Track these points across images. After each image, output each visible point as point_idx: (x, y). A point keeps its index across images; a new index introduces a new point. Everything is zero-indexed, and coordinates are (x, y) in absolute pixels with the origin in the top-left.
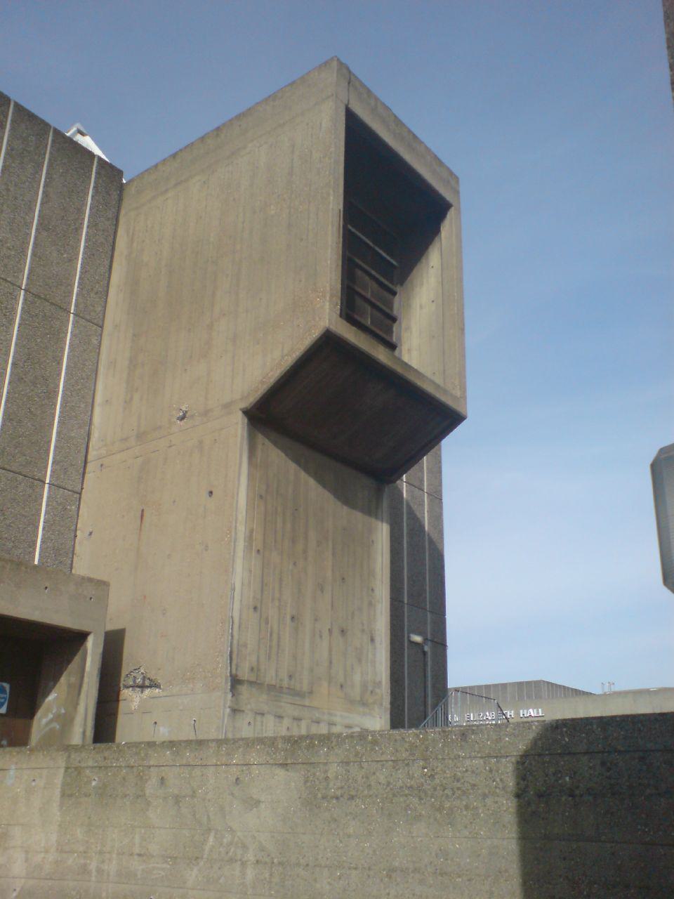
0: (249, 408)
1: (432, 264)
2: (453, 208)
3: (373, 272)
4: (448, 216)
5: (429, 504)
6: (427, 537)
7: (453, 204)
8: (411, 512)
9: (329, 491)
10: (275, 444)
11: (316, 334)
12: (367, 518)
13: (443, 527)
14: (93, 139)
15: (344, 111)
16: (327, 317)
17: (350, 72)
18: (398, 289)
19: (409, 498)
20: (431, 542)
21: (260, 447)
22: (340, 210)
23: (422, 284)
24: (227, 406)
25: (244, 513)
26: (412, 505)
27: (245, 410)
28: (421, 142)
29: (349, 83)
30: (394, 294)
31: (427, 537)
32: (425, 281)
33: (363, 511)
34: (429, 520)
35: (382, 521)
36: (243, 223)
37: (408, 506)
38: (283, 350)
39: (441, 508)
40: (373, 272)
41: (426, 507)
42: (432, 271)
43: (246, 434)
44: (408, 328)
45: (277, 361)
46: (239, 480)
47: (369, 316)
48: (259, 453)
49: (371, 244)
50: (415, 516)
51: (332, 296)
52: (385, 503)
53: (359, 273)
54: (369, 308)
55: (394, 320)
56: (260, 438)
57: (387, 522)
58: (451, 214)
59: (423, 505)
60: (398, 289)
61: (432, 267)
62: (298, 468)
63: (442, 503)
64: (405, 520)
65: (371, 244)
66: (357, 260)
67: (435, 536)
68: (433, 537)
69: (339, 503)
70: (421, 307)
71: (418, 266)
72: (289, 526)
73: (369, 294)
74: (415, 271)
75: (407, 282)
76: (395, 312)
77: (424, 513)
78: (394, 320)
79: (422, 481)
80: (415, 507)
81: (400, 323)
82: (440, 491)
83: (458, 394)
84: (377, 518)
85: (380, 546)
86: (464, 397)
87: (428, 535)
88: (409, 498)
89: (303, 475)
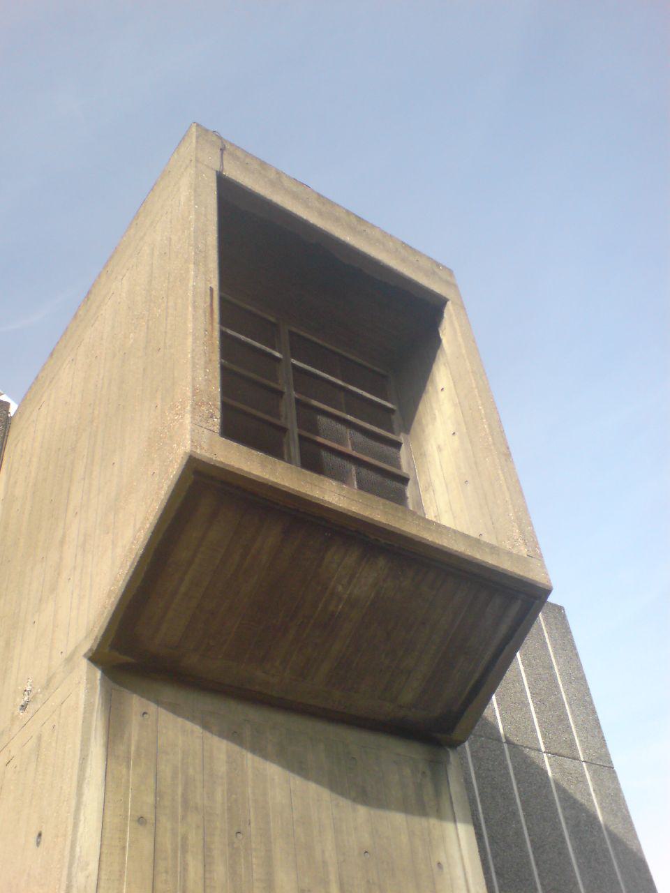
0: (95, 648)
1: (440, 387)
2: (449, 303)
3: (349, 417)
4: (445, 315)
5: (592, 778)
6: (605, 832)
7: (448, 297)
8: (567, 799)
9: (318, 782)
10: (175, 709)
11: (174, 470)
12: (418, 823)
13: (627, 810)
14: (7, 395)
15: (214, 185)
16: (188, 436)
17: (220, 138)
18: (402, 438)
19: (558, 776)
20: (616, 840)
21: (135, 721)
22: (211, 289)
23: (435, 418)
24: (69, 660)
25: (93, 866)
26: (565, 785)
27: (90, 655)
28: (373, 226)
29: (222, 150)
30: (398, 445)
31: (605, 832)
32: (437, 412)
33: (405, 808)
34: (601, 804)
35: (455, 821)
36: (103, 379)
37: (558, 786)
38: (134, 527)
39: (614, 778)
40: (349, 417)
41: (590, 782)
42: (442, 395)
43: (97, 700)
44: (429, 485)
45: (127, 548)
46: (80, 794)
47: (354, 478)
48: (134, 731)
49: (340, 382)
50: (576, 801)
51: (196, 406)
52: (455, 787)
53: (323, 420)
54: (353, 469)
55: (404, 480)
56: (136, 704)
57: (465, 822)
58: (449, 311)
59: (585, 782)
60: (402, 438)
61: (442, 389)
62: (236, 748)
63: (614, 772)
64: (560, 810)
65: (340, 382)
66: (315, 403)
67: (618, 829)
68: (616, 831)
69: (345, 803)
70: (440, 449)
71: (425, 397)
72: (220, 870)
73: (350, 448)
74: (421, 407)
75: (415, 424)
76: (405, 469)
77: (589, 795)
78: (404, 480)
79: (572, 745)
80: (571, 789)
81: (416, 483)
82: (607, 754)
83: (524, 551)
84: (440, 815)
85: (458, 871)
86: (536, 555)
87: (607, 829)
88: (558, 776)
89: (250, 760)
